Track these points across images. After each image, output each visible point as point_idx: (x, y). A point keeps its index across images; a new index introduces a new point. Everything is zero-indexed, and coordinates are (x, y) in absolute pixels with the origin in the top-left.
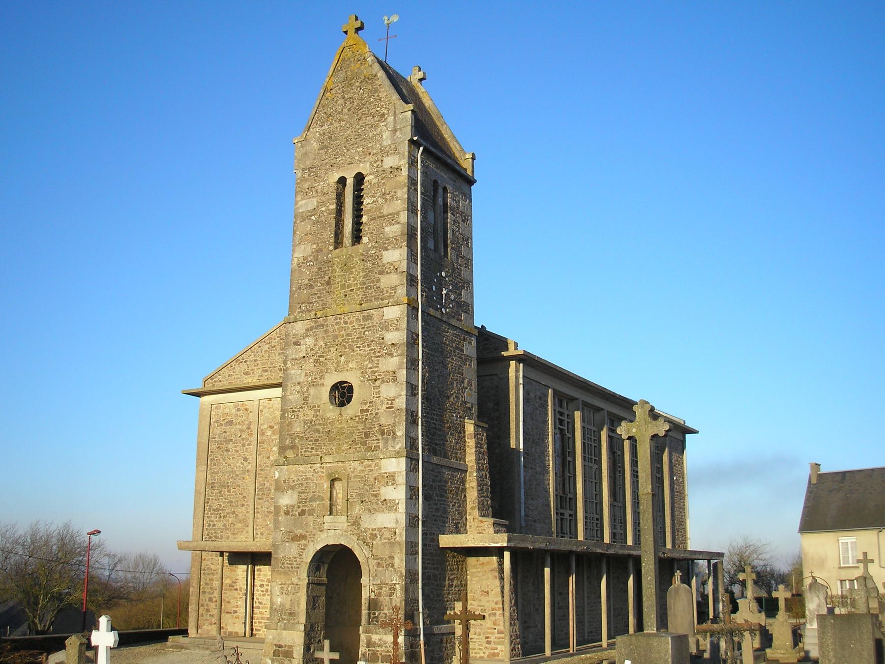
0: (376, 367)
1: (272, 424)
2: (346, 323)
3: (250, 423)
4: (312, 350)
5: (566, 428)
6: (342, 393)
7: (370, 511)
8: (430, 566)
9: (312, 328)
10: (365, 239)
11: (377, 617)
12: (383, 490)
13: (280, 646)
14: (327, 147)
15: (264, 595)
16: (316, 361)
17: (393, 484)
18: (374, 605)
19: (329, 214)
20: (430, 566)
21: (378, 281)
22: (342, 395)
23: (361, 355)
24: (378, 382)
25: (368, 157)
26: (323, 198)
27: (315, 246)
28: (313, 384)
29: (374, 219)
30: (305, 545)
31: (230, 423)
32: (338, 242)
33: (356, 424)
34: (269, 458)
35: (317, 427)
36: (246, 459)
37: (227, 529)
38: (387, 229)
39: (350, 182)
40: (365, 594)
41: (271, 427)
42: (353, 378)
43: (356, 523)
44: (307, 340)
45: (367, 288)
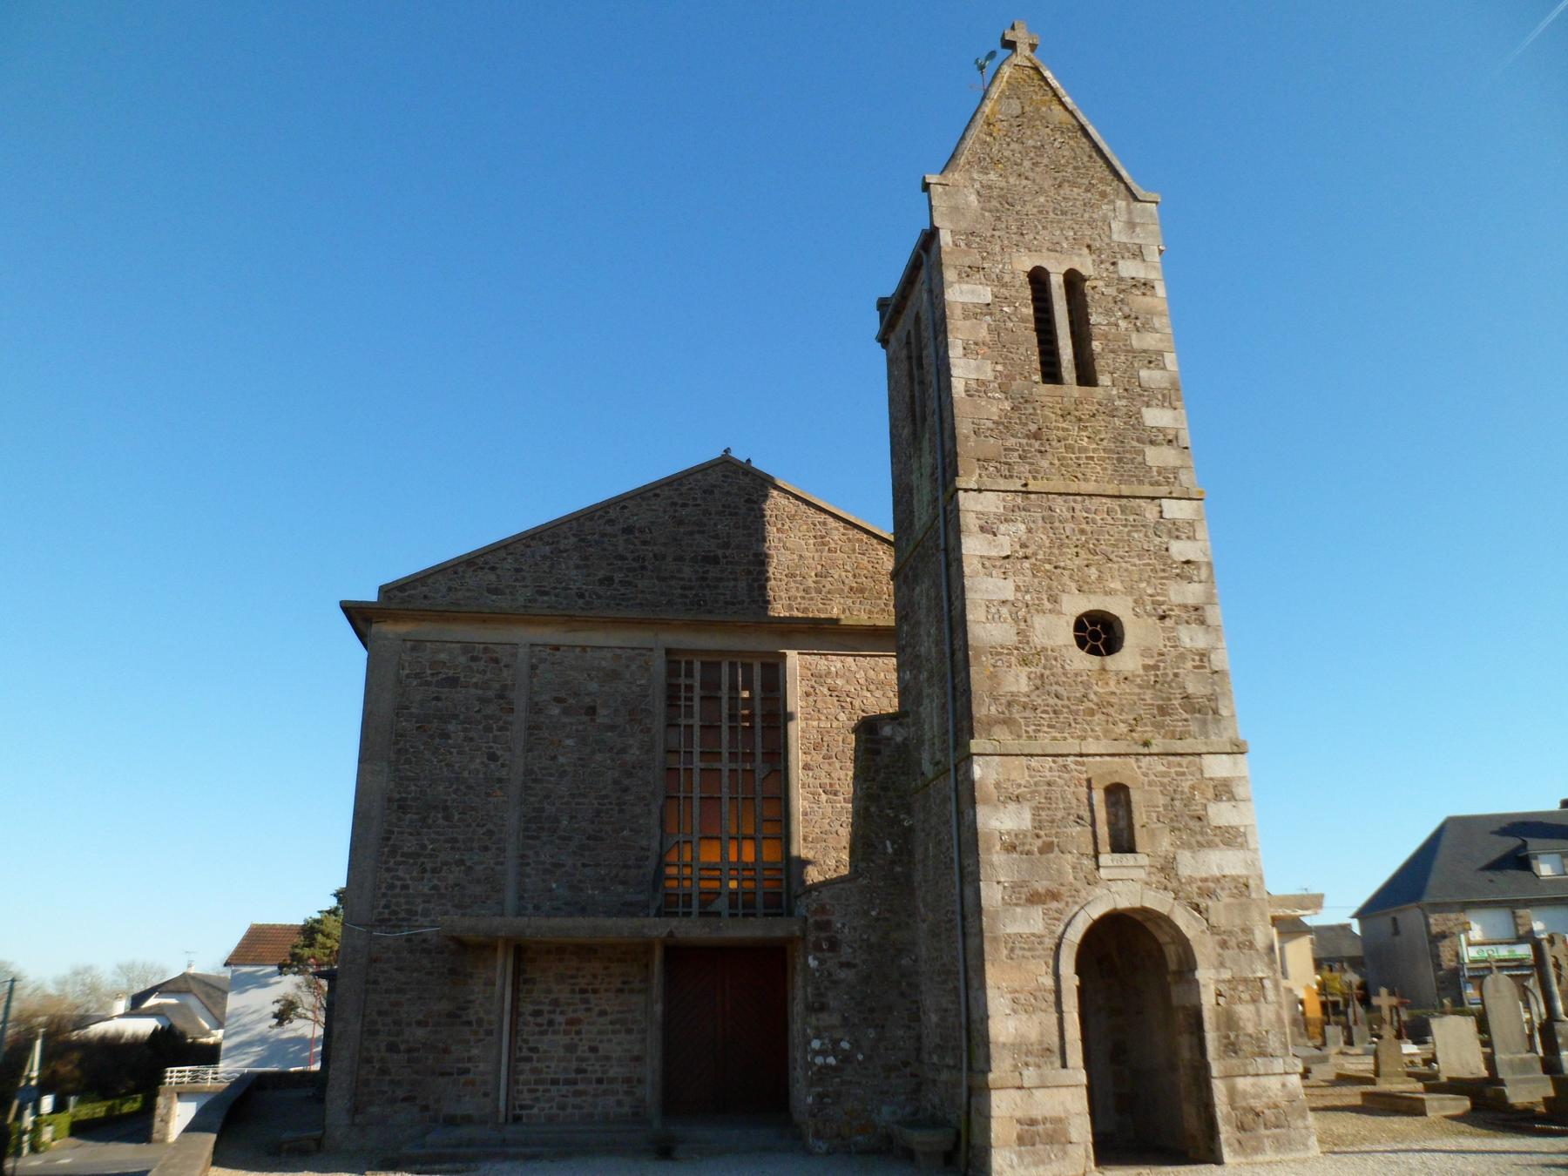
1: (563, 695)
6: (1099, 633)
10: (1104, 379)
13: (1033, 1122)
15: (542, 1033)
18: (1229, 1021)
27: (999, 368)
31: (453, 682)
32: (1051, 372)
33: (1137, 690)
34: (554, 758)
37: (442, 896)
38: (1144, 373)
40: (1208, 1000)
41: (558, 700)
42: (1118, 607)
43: (1167, 868)
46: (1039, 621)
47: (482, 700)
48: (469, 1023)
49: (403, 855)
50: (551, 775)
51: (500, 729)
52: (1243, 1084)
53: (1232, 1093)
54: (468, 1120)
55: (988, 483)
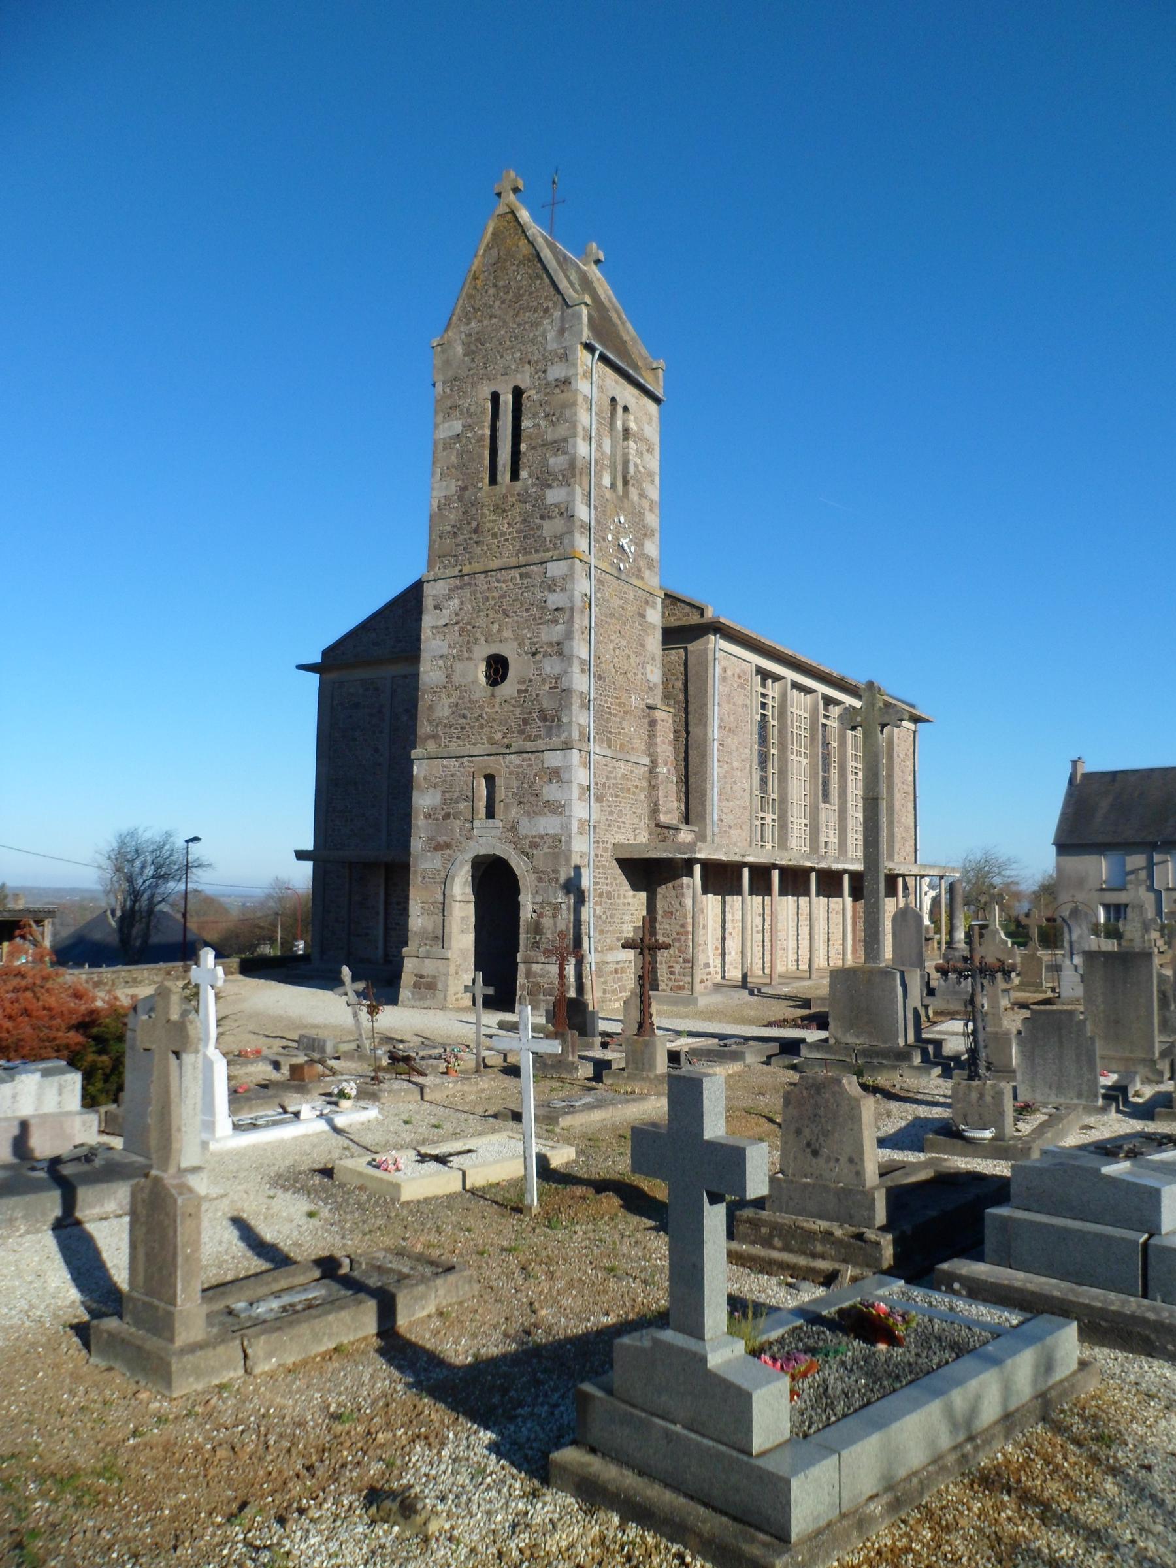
13: (422, 977)
16: (461, 630)
18: (537, 928)
29: (534, 448)
42: (508, 650)
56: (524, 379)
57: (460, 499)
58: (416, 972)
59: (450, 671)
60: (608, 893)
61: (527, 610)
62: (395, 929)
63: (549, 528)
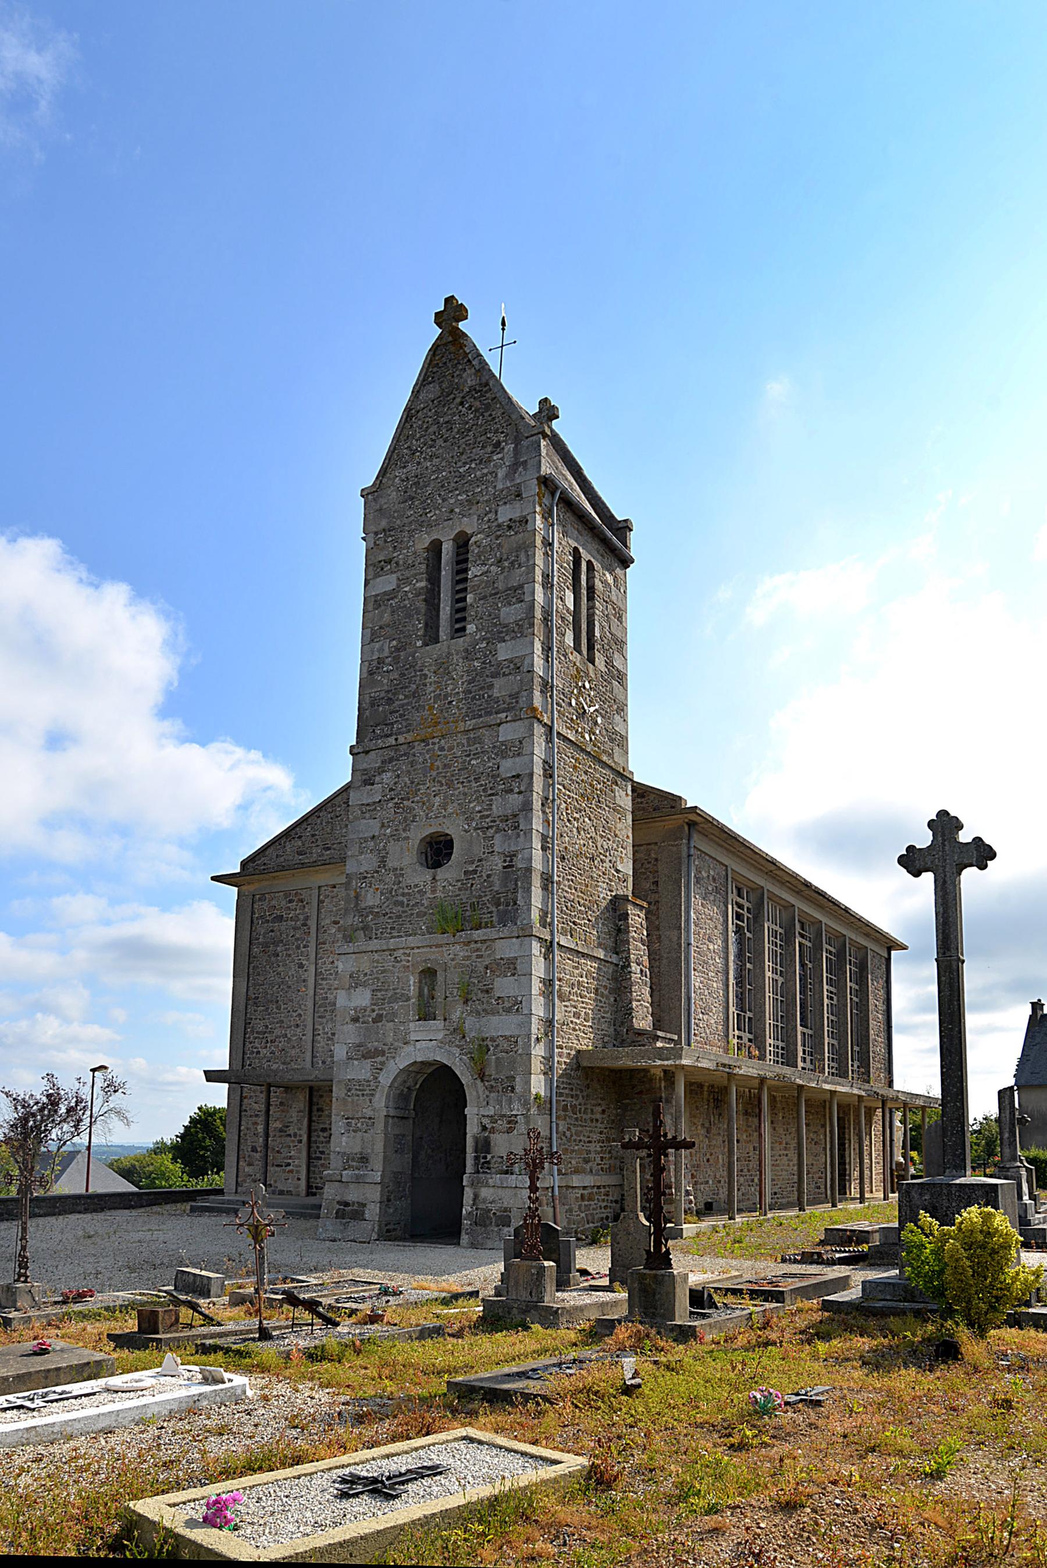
0: (487, 810)
2: (442, 749)
3: (307, 918)
4: (391, 790)
5: (745, 925)
7: (478, 1013)
8: (567, 1091)
9: (391, 760)
11: (488, 1162)
12: (499, 982)
13: (347, 1204)
14: (412, 498)
16: (397, 806)
17: (513, 975)
18: (484, 1146)
19: (417, 595)
20: (567, 1091)
21: (491, 686)
22: (438, 853)
23: (465, 794)
24: (492, 831)
25: (474, 508)
26: (407, 573)
27: (394, 643)
28: (395, 837)
29: (484, 598)
30: (383, 1063)
35: (400, 898)
36: (301, 966)
39: (447, 548)
40: (472, 1129)
42: (454, 828)
44: (384, 776)
45: (474, 698)
46: (393, 847)
47: (295, 929)
48: (290, 1135)
49: (257, 1033)
50: (331, 974)
51: (305, 947)
52: (485, 1193)
53: (476, 1196)
54: (289, 1193)
55: (372, 745)
56: (469, 525)
57: (396, 660)
58: (338, 1198)
59: (383, 853)
60: (574, 1107)
61: (477, 780)
62: (320, 1159)
63: (500, 688)
